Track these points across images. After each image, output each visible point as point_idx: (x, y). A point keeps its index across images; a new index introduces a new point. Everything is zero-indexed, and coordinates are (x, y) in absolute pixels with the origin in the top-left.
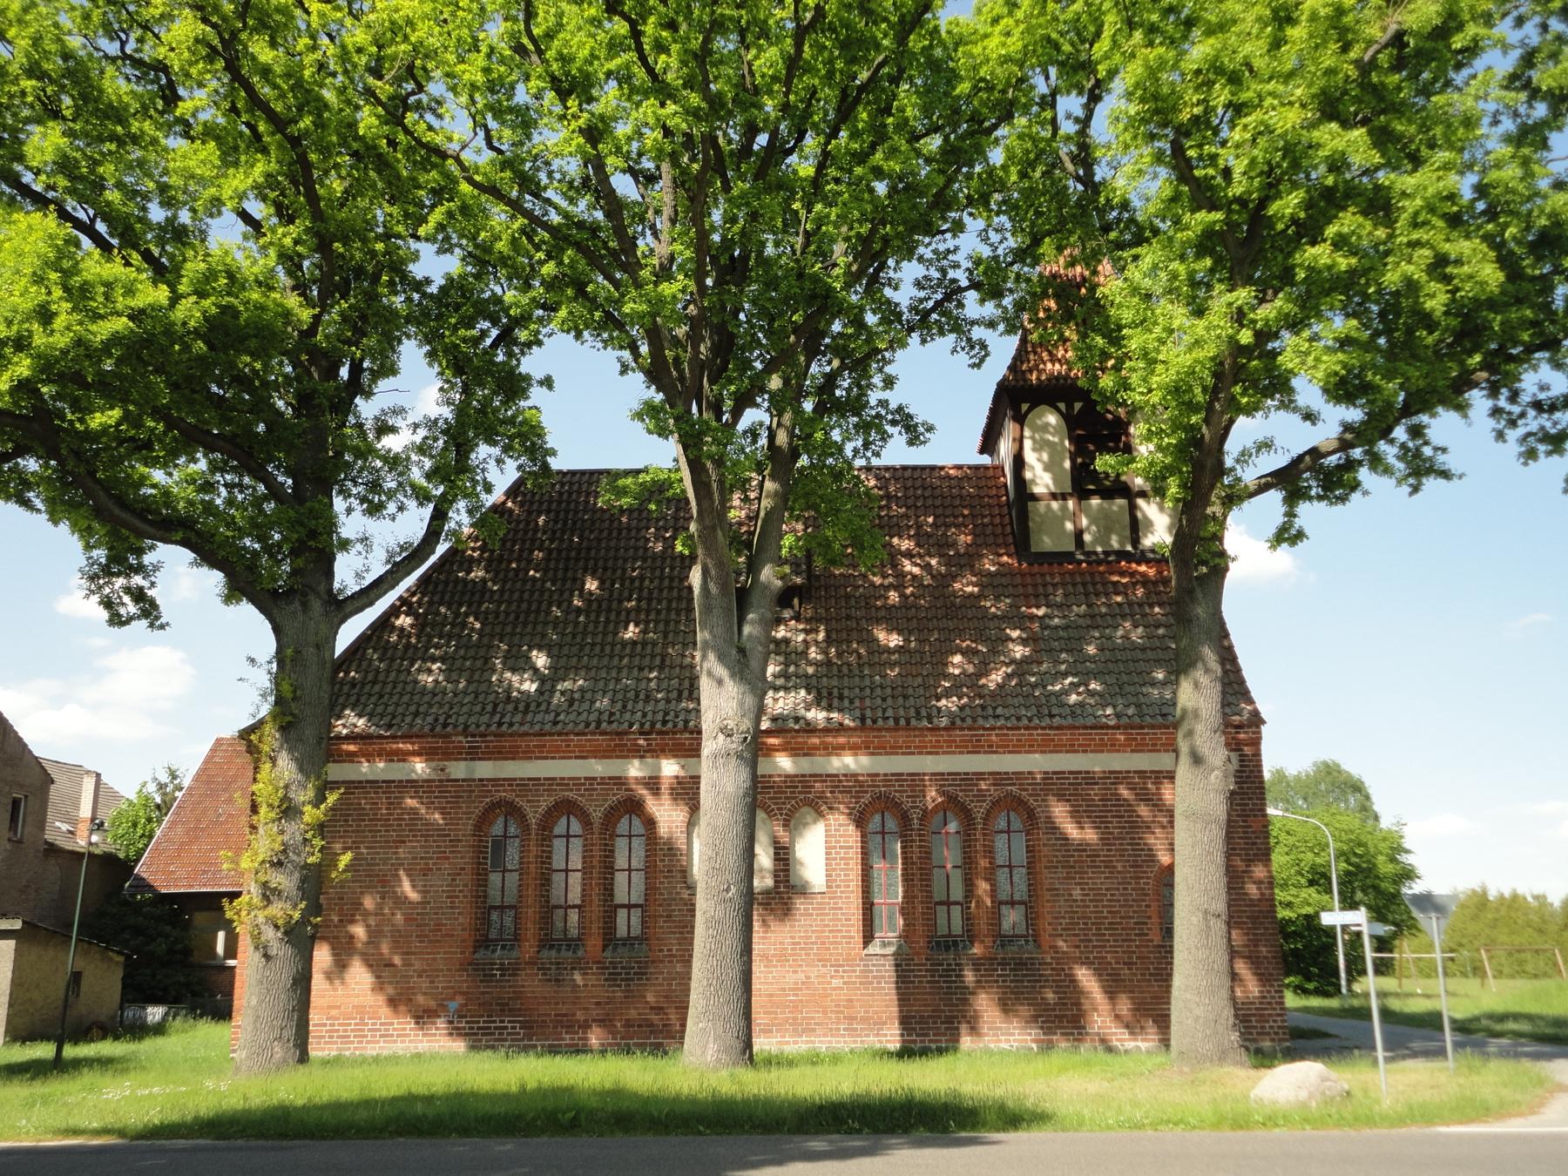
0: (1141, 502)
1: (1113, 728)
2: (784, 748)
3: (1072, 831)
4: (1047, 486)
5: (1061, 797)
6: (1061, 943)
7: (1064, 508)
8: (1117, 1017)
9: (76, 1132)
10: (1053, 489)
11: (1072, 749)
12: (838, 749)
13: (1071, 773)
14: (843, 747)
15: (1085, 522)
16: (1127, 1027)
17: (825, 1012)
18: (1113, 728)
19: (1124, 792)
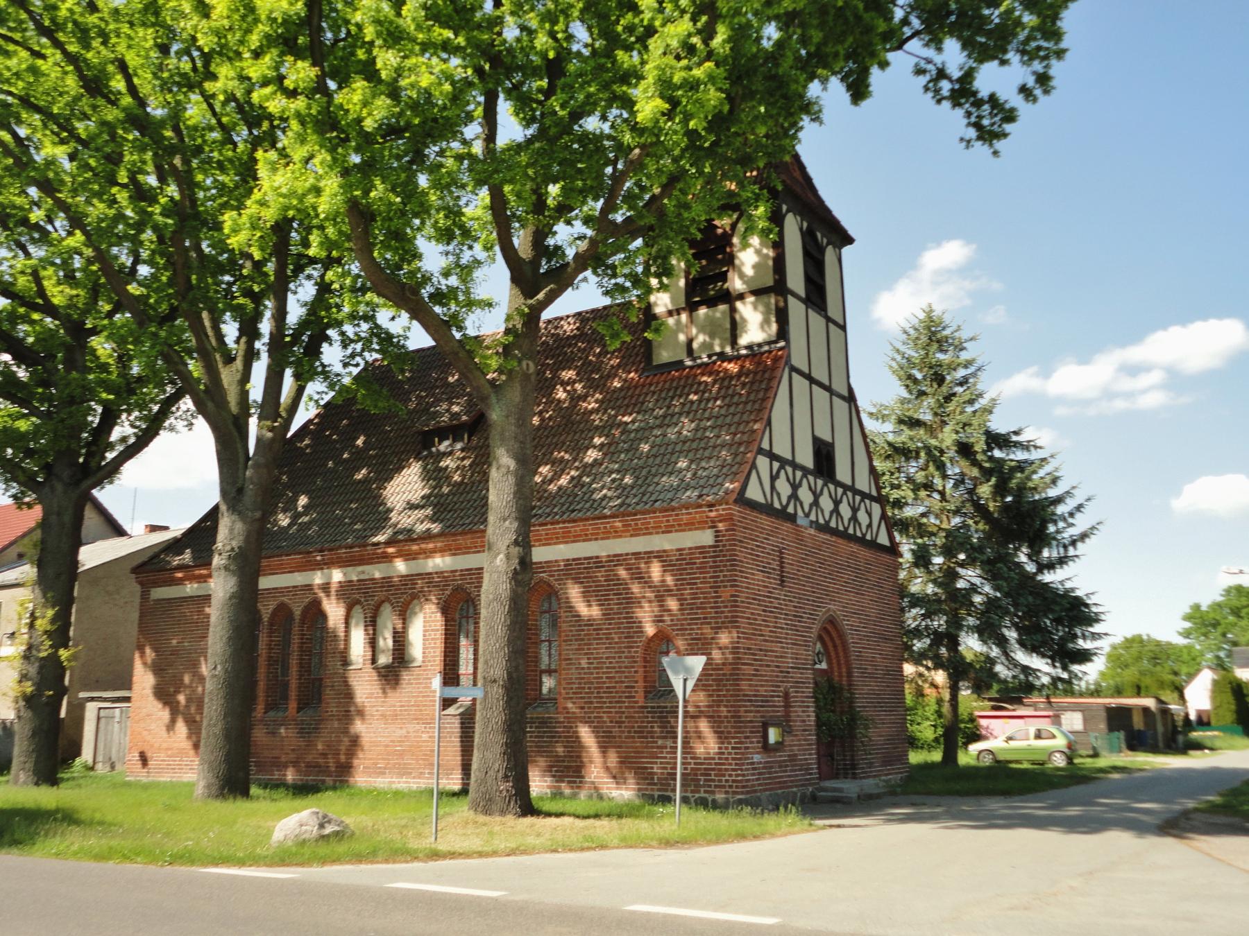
0: (739, 305)
1: (610, 517)
2: (399, 554)
3: (583, 609)
4: (666, 305)
5: (577, 580)
6: (570, 705)
7: (678, 322)
8: (607, 769)
9: (839, 826)
10: (670, 307)
11: (576, 539)
12: (429, 554)
13: (586, 559)
14: (434, 551)
15: (694, 331)
16: (614, 777)
17: (417, 760)
18: (610, 517)
19: (623, 573)
